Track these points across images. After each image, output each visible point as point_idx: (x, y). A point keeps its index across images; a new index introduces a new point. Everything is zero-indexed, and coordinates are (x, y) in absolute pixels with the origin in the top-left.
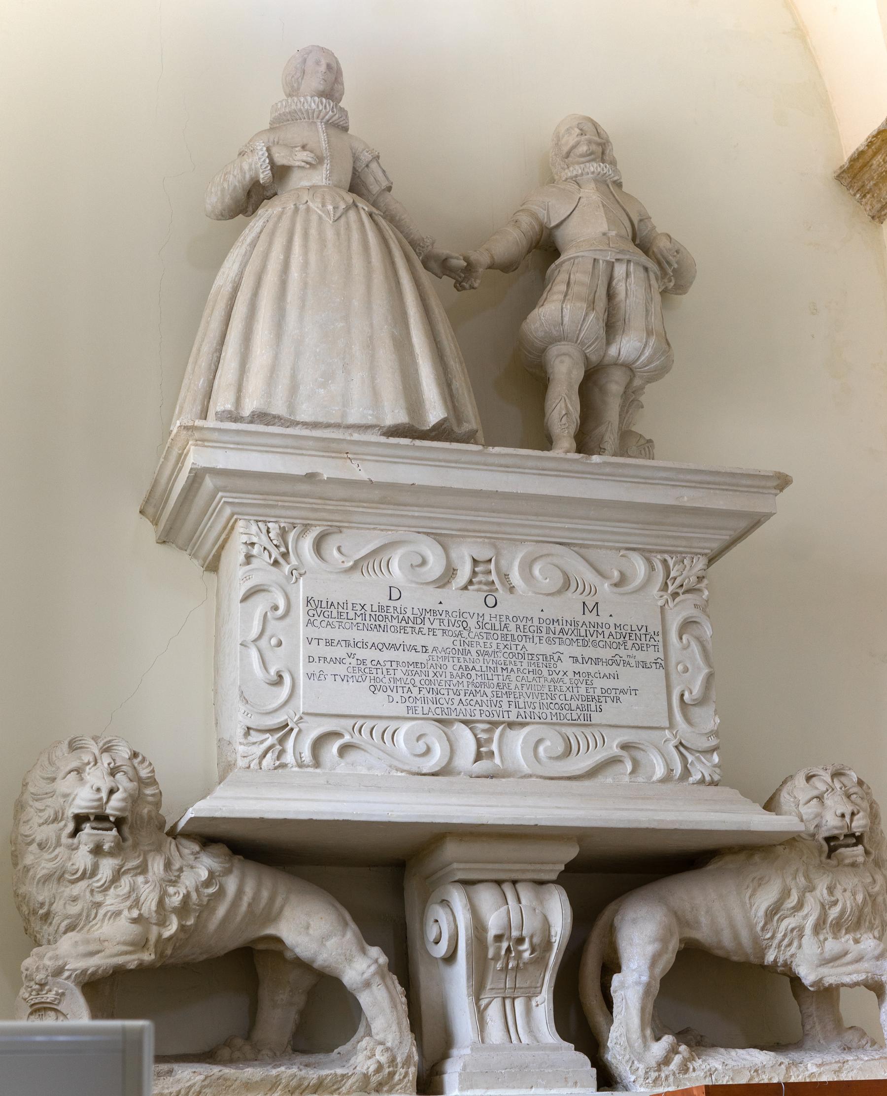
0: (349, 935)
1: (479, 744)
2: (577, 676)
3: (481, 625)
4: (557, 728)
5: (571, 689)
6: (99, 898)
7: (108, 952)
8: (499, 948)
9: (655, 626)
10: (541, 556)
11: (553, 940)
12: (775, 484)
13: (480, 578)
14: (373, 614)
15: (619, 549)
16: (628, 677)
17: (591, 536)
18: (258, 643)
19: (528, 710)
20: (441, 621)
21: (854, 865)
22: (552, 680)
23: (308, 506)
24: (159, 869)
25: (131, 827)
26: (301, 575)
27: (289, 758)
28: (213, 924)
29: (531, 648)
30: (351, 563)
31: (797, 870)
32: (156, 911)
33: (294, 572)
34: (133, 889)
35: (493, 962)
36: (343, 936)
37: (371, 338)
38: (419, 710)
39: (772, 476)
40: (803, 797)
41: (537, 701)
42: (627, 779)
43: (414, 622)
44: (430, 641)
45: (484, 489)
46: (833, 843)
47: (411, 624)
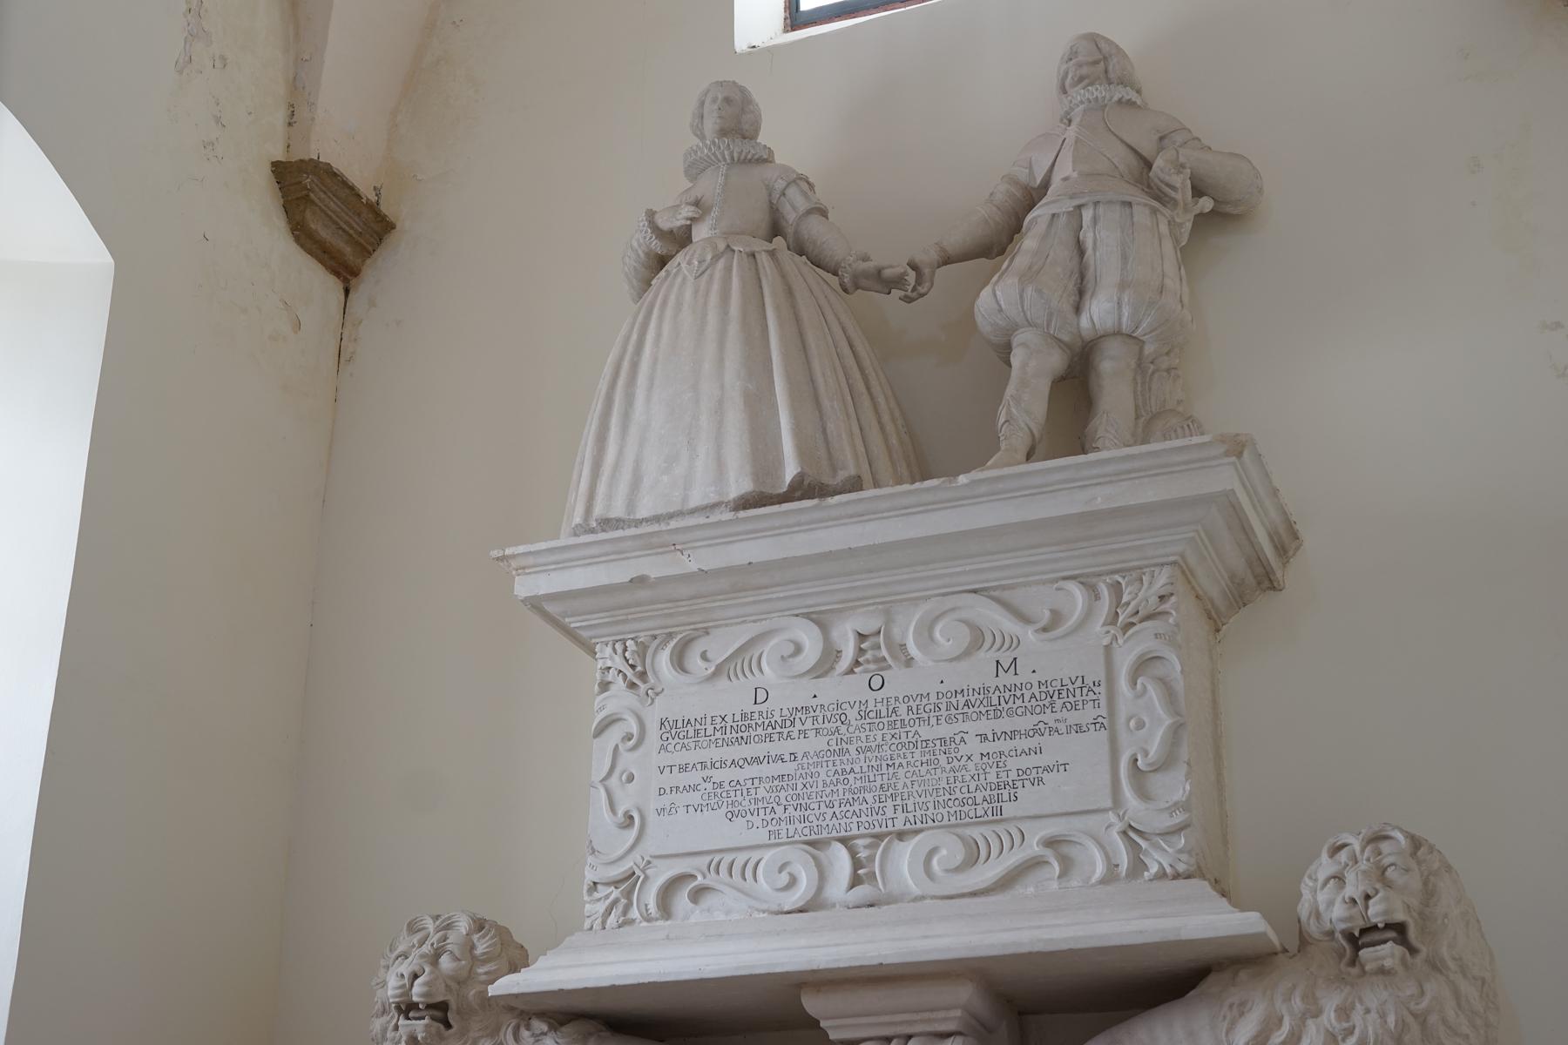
1: (857, 864)
4: (959, 831)
9: (1096, 672)
10: (945, 613)
12: (1222, 450)
13: (869, 655)
15: (1056, 580)
16: (1055, 748)
19: (918, 814)
20: (815, 719)
21: (1382, 971)
25: (459, 1012)
27: (634, 913)
29: (925, 732)
31: (1294, 987)
37: (721, 402)
38: (783, 833)
40: (1321, 877)
42: (1055, 885)
43: (780, 727)
44: (799, 746)
46: (1359, 938)
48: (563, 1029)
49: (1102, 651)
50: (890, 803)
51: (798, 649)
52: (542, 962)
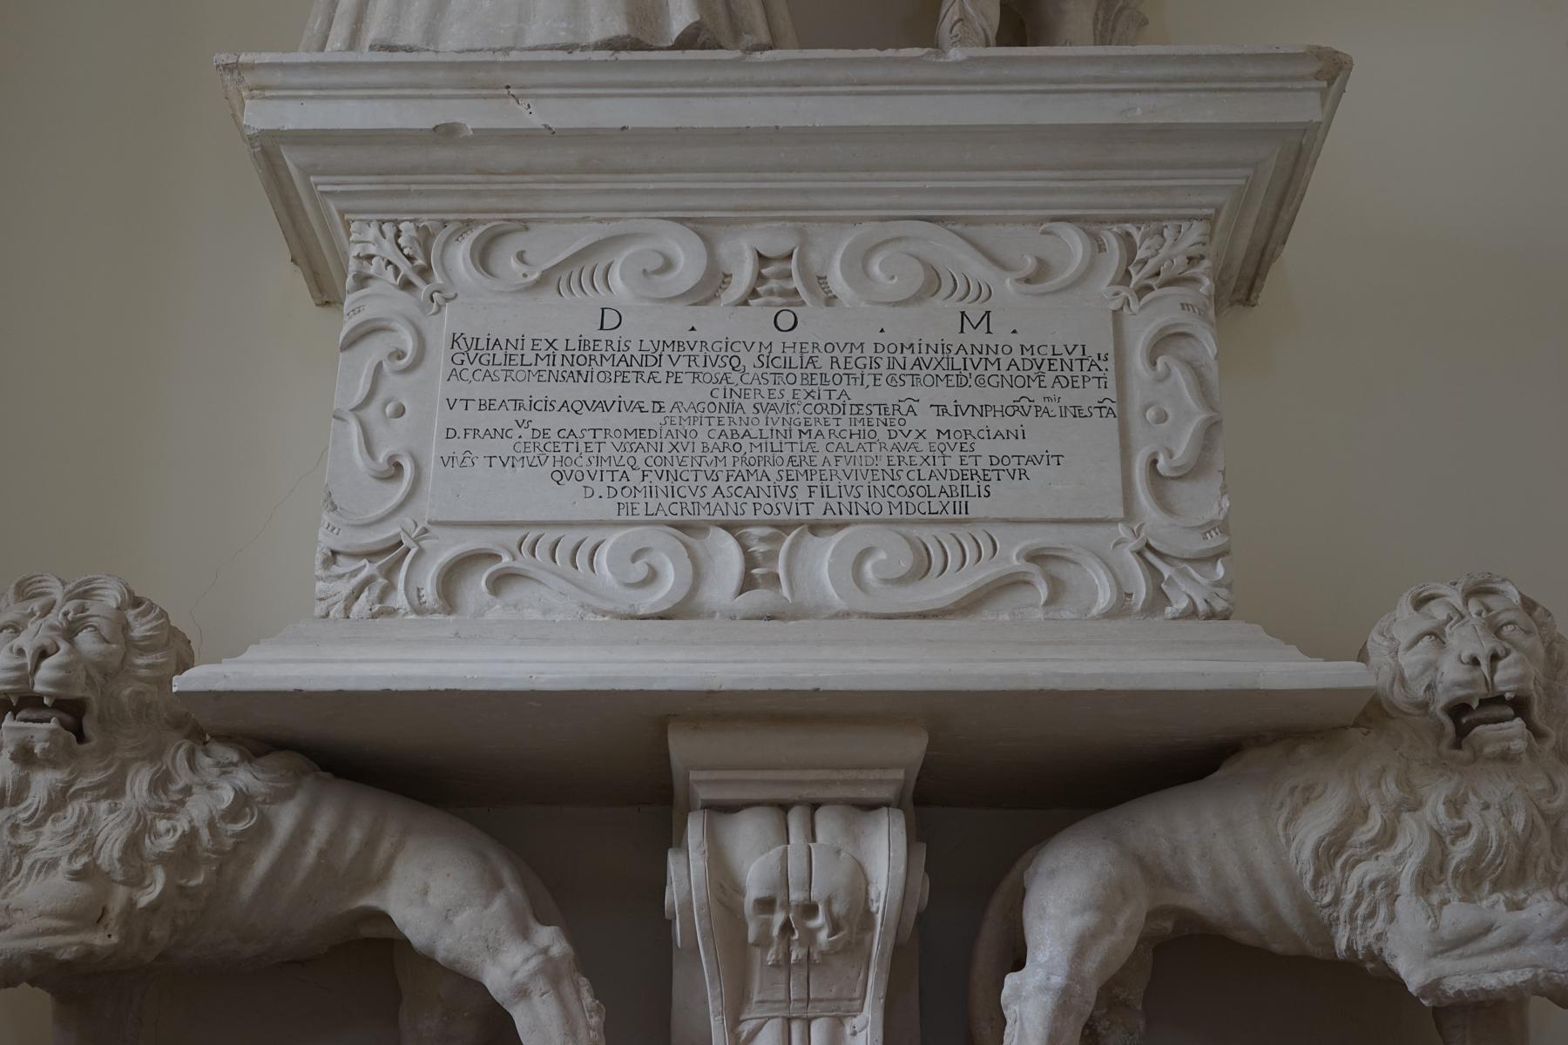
0: (498, 904)
1: (750, 561)
2: (944, 438)
3: (765, 361)
4: (903, 529)
5: (930, 460)
6: (25, 838)
7: (17, 929)
8: (767, 925)
10: (886, 242)
11: (874, 909)
13: (773, 284)
14: (568, 354)
15: (1039, 221)
16: (1042, 435)
17: (976, 201)
18: (361, 413)
19: (845, 500)
20: (692, 359)
21: (1506, 757)
22: (896, 447)
23: (462, 187)
24: (140, 789)
26: (447, 300)
27: (399, 599)
28: (248, 887)
29: (856, 394)
30: (536, 276)
31: (1384, 770)
32: (120, 860)
33: (435, 295)
34: (84, 821)
35: (758, 952)
36: (486, 906)
38: (640, 508)
39: (1304, 55)
40: (1404, 636)
41: (865, 484)
42: (1039, 614)
44: (667, 393)
45: (752, 125)
47: (636, 367)
48: (262, 760)
49: (1110, 316)
50: (803, 483)
51: (668, 265)
52: (252, 653)
